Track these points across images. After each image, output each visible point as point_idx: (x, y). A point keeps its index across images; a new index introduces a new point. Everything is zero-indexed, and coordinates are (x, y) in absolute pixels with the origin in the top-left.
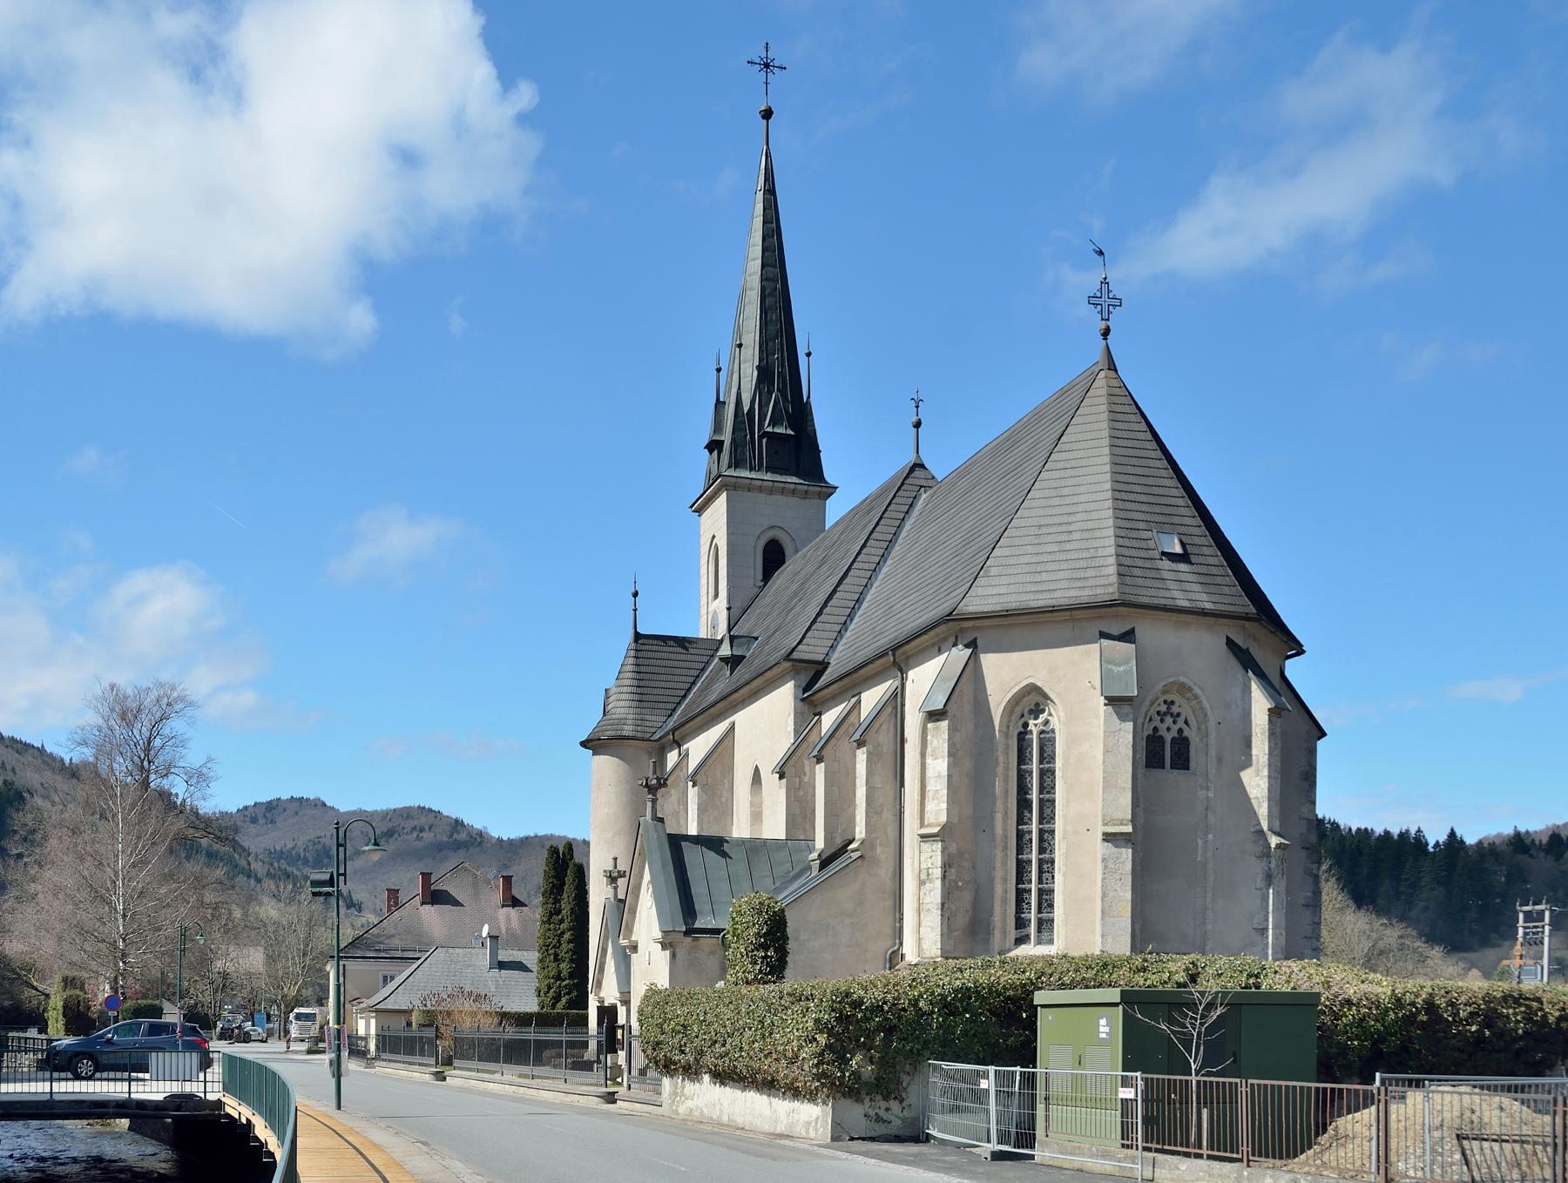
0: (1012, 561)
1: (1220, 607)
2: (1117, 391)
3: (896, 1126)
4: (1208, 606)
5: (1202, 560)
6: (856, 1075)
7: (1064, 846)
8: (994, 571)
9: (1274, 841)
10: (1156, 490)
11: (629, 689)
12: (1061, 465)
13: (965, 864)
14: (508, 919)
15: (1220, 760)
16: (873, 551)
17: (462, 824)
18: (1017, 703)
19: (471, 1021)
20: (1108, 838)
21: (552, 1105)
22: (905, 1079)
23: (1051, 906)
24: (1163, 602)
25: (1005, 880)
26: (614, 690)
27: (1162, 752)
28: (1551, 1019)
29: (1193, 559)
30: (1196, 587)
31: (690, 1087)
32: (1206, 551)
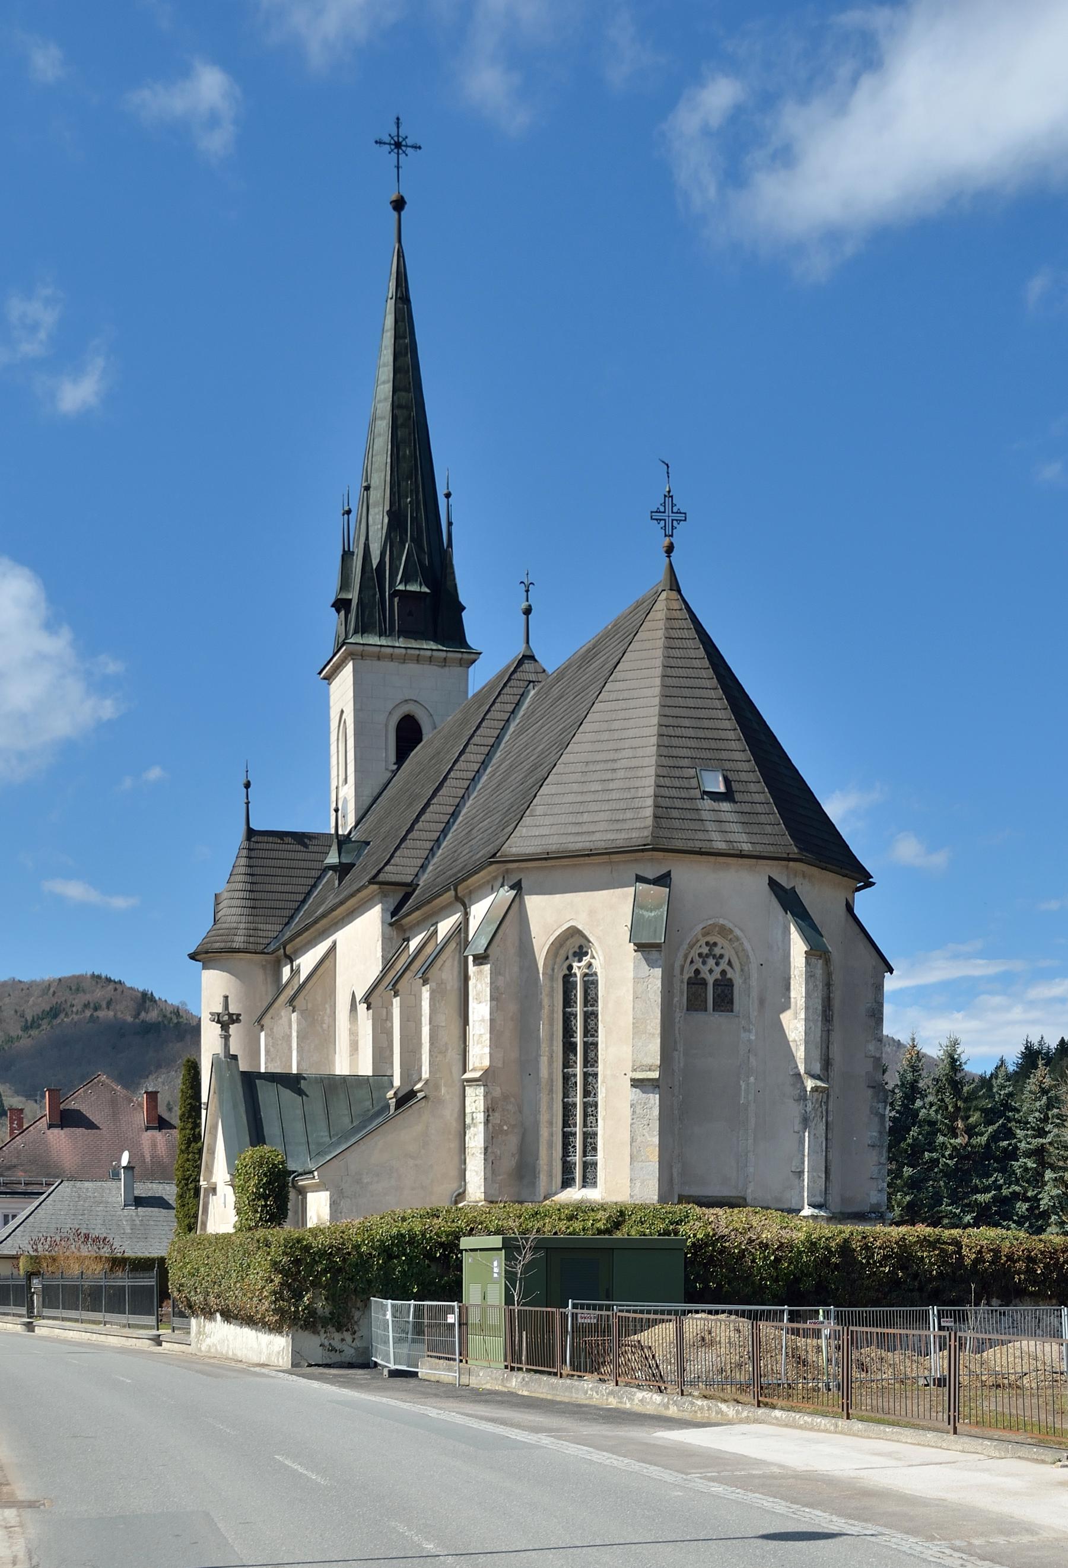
0: (556, 800)
1: (759, 848)
2: (678, 614)
3: (349, 1353)
4: (746, 847)
5: (747, 797)
6: (311, 1311)
7: (604, 1090)
8: (540, 810)
9: (810, 1084)
10: (706, 724)
11: (241, 894)
12: (613, 696)
13: (510, 1107)
14: (154, 1145)
15: (762, 1002)
16: (472, 757)
17: (152, 999)
18: (561, 946)
19: (81, 1264)
20: (636, 1083)
21: (80, 1344)
22: (357, 1314)
23: (595, 1149)
24: (698, 844)
25: (551, 1123)
26: (226, 895)
27: (703, 992)
28: (967, 1262)
29: (738, 797)
30: (735, 827)
31: (210, 1326)
32: (753, 787)
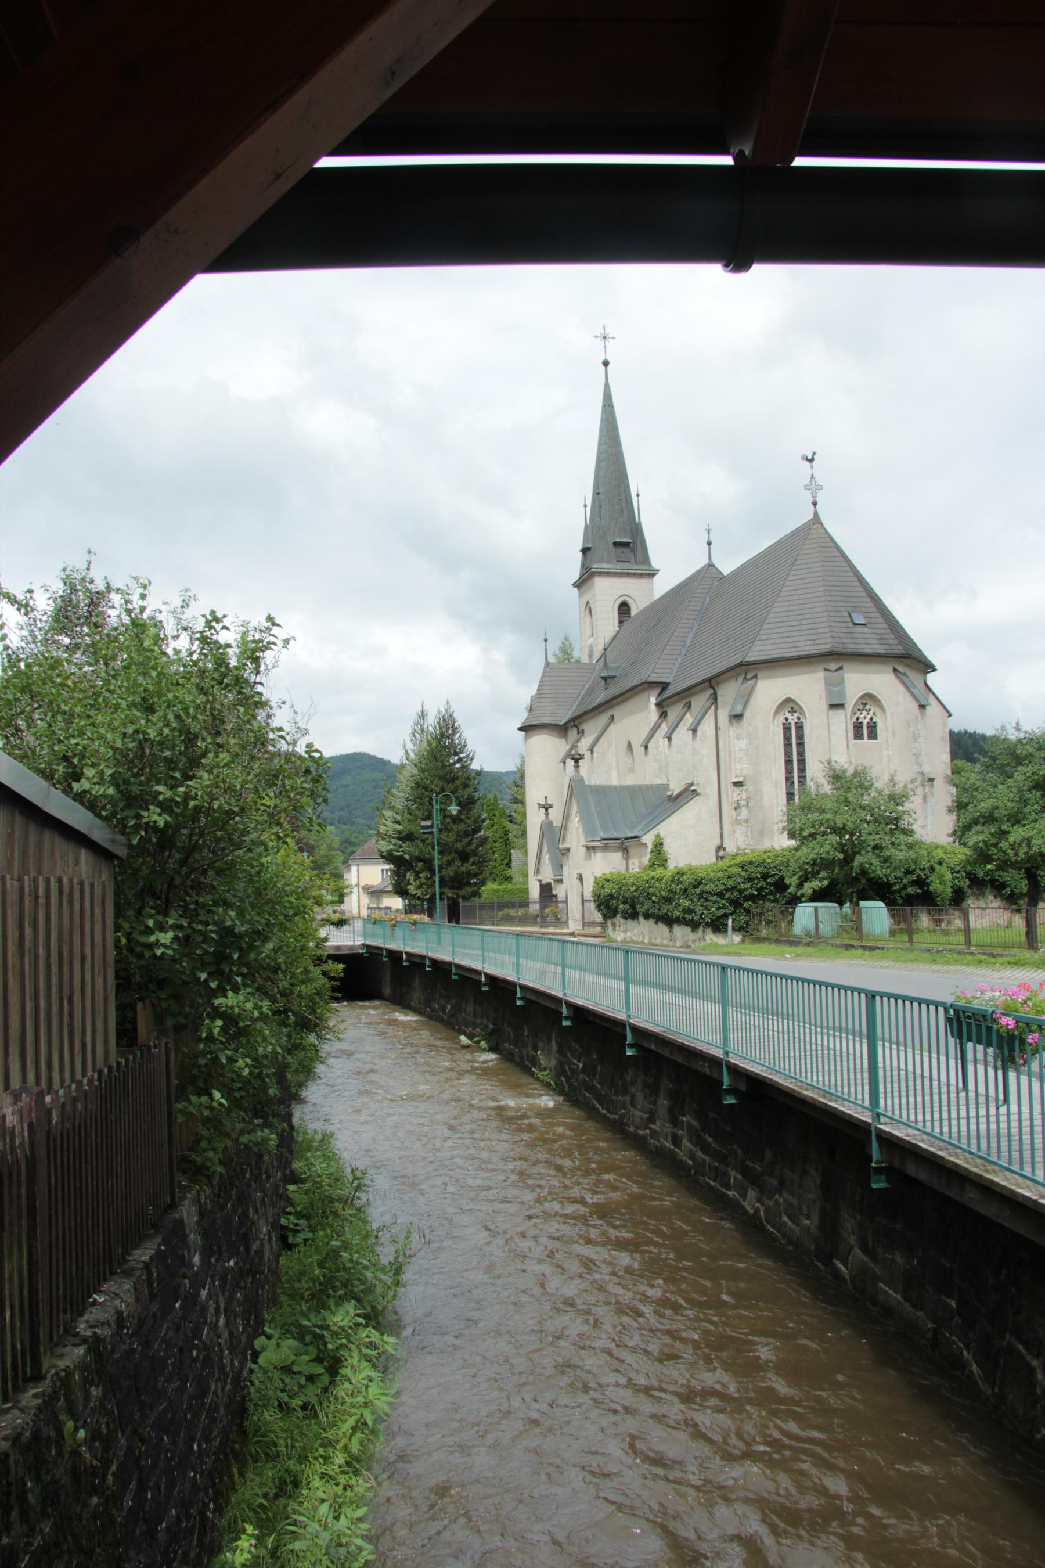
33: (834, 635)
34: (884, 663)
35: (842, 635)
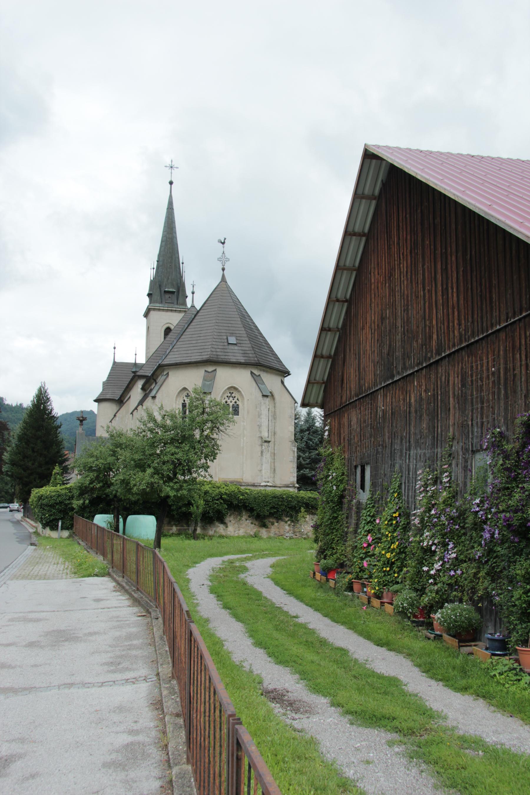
15: (248, 412)
33: (213, 350)
34: (245, 368)
35: (218, 350)
